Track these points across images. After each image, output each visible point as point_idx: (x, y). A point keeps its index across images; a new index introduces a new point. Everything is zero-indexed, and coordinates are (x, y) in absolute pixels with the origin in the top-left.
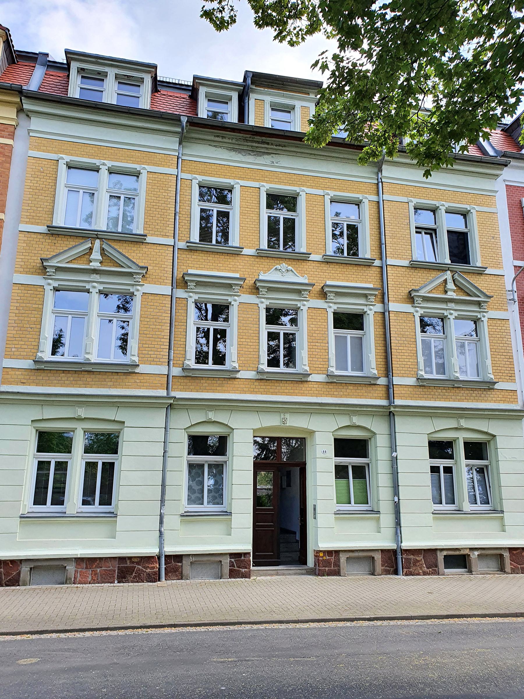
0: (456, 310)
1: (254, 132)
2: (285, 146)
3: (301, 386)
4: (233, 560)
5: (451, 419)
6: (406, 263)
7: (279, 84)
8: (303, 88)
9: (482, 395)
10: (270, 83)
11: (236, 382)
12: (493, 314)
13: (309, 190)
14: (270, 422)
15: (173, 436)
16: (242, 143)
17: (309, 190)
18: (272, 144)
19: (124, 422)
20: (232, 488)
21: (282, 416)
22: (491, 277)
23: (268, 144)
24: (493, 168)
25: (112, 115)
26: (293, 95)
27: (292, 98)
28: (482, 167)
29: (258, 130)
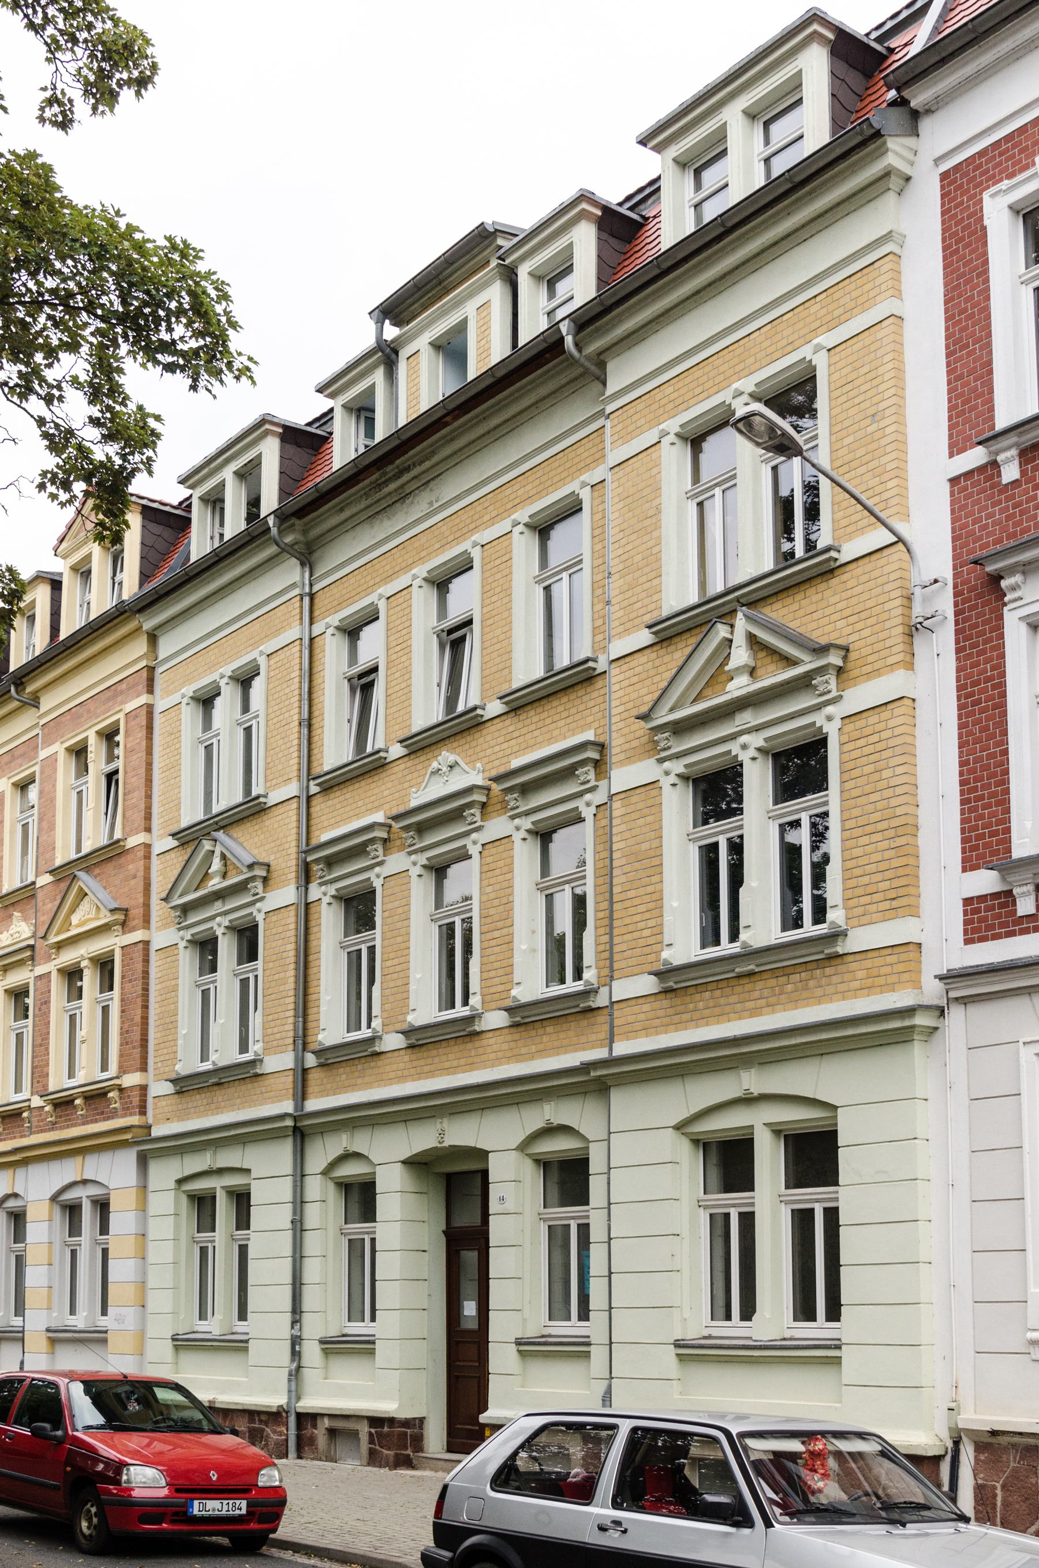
0: (757, 729)
1: (454, 410)
2: (433, 453)
3: (469, 1046)
4: (373, 1431)
5: (727, 1072)
6: (645, 637)
7: (433, 288)
8: (473, 258)
9: (812, 983)
10: (422, 297)
11: (381, 1062)
12: (860, 696)
13: (828, 339)
14: (423, 1139)
15: (315, 1187)
16: (378, 496)
17: (828, 339)
18: (414, 465)
19: (248, 1171)
20: (50, 1279)
21: (439, 1126)
22: (865, 566)
23: (408, 469)
24: (854, 169)
25: (223, 567)
26: (466, 289)
27: (444, 313)
28: (812, 195)
29: (463, 399)
